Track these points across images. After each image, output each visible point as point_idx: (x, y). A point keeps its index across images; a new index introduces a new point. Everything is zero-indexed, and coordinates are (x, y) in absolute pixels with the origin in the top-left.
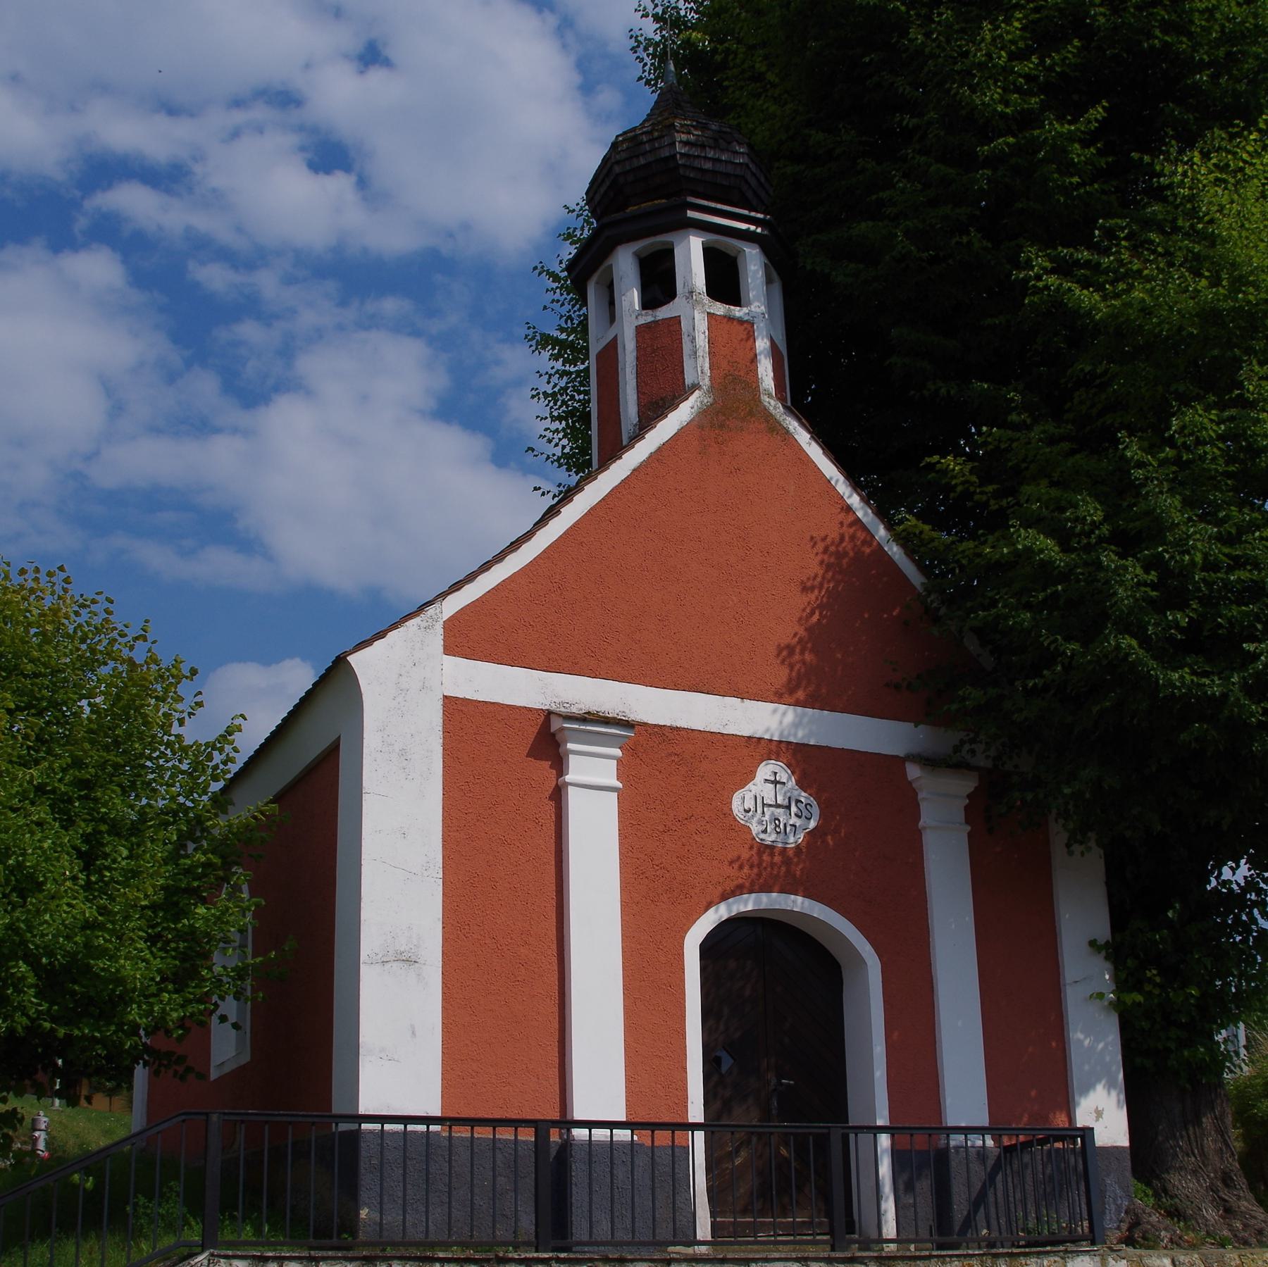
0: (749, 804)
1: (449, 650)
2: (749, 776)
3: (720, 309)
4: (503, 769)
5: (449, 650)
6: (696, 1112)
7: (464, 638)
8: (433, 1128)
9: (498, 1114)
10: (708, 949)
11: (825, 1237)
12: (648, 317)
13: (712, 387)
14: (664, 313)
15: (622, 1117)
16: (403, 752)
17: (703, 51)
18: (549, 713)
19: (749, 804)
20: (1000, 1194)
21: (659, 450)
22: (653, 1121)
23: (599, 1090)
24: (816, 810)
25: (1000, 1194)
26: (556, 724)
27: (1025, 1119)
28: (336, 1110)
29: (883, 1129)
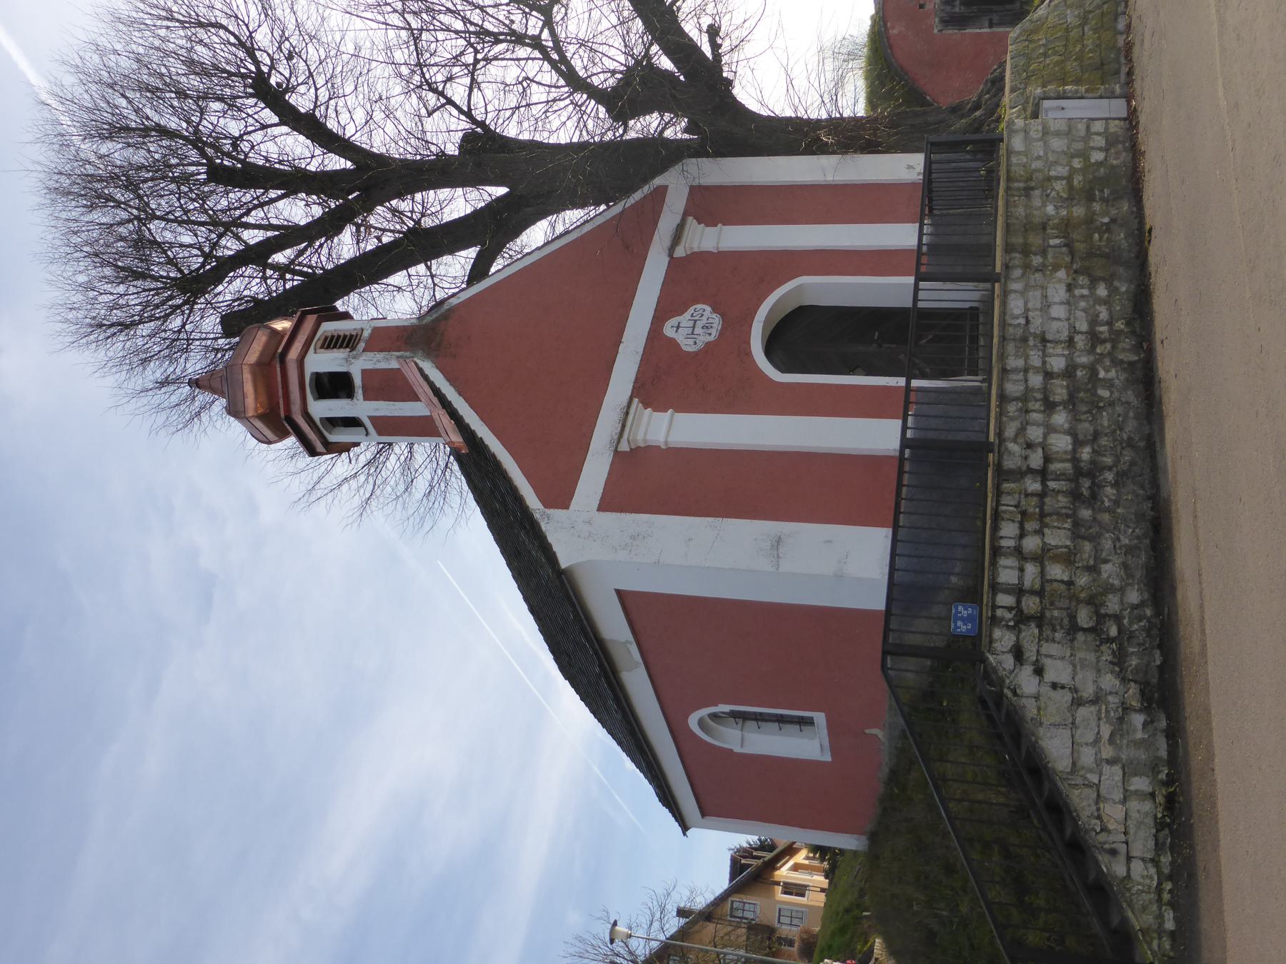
0: (691, 342)
1: (566, 506)
2: (673, 342)
3: (362, 345)
4: (649, 484)
5: (566, 506)
6: (901, 381)
7: (560, 496)
8: (909, 424)
9: (881, 629)
10: (784, 369)
11: (1004, 508)
12: (359, 392)
13: (411, 351)
14: (358, 381)
15: (900, 422)
16: (633, 537)
17: (262, 300)
18: (616, 452)
19: (691, 342)
20: (966, 165)
21: (448, 380)
22: (903, 404)
23: (881, 436)
24: (699, 306)
25: (966, 165)
26: (624, 447)
27: (875, 731)
28: (909, 304)
29: (908, 383)
